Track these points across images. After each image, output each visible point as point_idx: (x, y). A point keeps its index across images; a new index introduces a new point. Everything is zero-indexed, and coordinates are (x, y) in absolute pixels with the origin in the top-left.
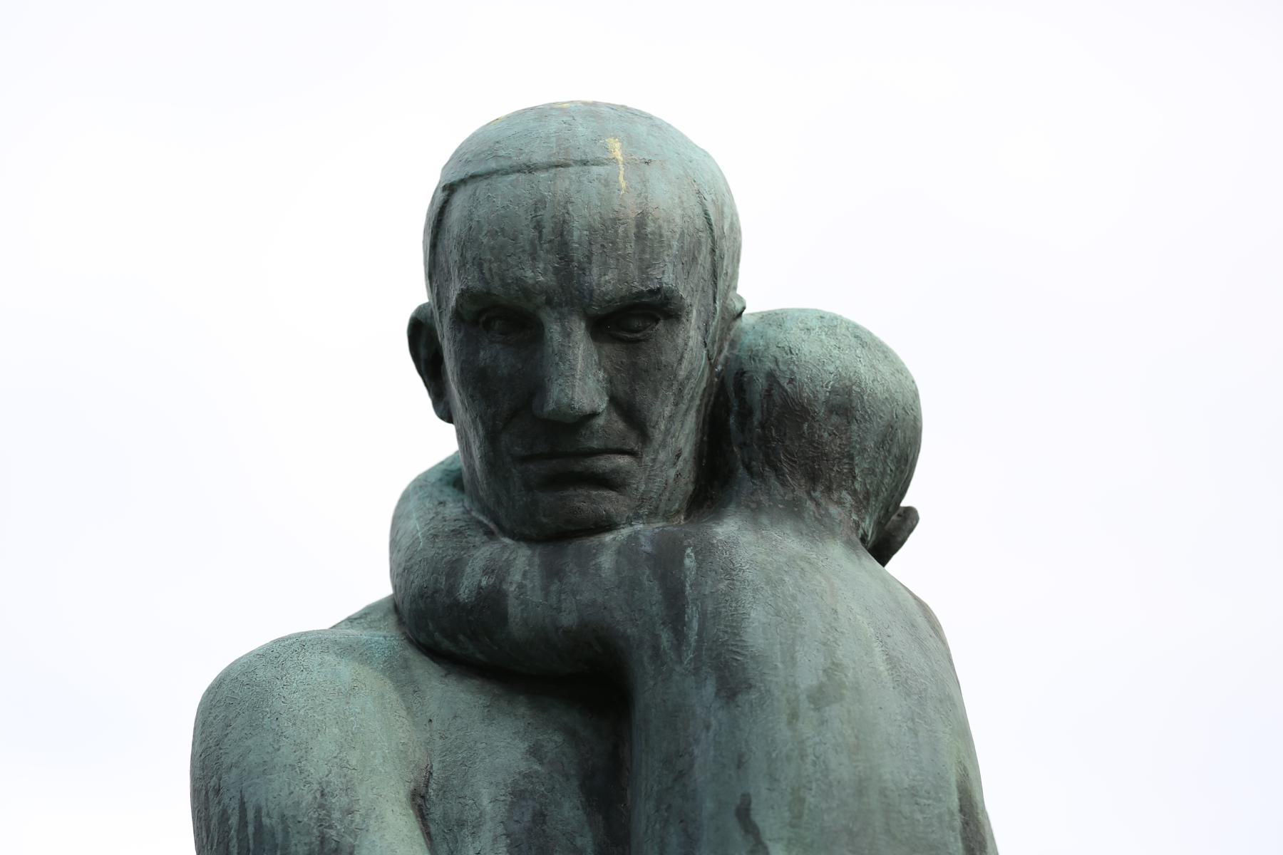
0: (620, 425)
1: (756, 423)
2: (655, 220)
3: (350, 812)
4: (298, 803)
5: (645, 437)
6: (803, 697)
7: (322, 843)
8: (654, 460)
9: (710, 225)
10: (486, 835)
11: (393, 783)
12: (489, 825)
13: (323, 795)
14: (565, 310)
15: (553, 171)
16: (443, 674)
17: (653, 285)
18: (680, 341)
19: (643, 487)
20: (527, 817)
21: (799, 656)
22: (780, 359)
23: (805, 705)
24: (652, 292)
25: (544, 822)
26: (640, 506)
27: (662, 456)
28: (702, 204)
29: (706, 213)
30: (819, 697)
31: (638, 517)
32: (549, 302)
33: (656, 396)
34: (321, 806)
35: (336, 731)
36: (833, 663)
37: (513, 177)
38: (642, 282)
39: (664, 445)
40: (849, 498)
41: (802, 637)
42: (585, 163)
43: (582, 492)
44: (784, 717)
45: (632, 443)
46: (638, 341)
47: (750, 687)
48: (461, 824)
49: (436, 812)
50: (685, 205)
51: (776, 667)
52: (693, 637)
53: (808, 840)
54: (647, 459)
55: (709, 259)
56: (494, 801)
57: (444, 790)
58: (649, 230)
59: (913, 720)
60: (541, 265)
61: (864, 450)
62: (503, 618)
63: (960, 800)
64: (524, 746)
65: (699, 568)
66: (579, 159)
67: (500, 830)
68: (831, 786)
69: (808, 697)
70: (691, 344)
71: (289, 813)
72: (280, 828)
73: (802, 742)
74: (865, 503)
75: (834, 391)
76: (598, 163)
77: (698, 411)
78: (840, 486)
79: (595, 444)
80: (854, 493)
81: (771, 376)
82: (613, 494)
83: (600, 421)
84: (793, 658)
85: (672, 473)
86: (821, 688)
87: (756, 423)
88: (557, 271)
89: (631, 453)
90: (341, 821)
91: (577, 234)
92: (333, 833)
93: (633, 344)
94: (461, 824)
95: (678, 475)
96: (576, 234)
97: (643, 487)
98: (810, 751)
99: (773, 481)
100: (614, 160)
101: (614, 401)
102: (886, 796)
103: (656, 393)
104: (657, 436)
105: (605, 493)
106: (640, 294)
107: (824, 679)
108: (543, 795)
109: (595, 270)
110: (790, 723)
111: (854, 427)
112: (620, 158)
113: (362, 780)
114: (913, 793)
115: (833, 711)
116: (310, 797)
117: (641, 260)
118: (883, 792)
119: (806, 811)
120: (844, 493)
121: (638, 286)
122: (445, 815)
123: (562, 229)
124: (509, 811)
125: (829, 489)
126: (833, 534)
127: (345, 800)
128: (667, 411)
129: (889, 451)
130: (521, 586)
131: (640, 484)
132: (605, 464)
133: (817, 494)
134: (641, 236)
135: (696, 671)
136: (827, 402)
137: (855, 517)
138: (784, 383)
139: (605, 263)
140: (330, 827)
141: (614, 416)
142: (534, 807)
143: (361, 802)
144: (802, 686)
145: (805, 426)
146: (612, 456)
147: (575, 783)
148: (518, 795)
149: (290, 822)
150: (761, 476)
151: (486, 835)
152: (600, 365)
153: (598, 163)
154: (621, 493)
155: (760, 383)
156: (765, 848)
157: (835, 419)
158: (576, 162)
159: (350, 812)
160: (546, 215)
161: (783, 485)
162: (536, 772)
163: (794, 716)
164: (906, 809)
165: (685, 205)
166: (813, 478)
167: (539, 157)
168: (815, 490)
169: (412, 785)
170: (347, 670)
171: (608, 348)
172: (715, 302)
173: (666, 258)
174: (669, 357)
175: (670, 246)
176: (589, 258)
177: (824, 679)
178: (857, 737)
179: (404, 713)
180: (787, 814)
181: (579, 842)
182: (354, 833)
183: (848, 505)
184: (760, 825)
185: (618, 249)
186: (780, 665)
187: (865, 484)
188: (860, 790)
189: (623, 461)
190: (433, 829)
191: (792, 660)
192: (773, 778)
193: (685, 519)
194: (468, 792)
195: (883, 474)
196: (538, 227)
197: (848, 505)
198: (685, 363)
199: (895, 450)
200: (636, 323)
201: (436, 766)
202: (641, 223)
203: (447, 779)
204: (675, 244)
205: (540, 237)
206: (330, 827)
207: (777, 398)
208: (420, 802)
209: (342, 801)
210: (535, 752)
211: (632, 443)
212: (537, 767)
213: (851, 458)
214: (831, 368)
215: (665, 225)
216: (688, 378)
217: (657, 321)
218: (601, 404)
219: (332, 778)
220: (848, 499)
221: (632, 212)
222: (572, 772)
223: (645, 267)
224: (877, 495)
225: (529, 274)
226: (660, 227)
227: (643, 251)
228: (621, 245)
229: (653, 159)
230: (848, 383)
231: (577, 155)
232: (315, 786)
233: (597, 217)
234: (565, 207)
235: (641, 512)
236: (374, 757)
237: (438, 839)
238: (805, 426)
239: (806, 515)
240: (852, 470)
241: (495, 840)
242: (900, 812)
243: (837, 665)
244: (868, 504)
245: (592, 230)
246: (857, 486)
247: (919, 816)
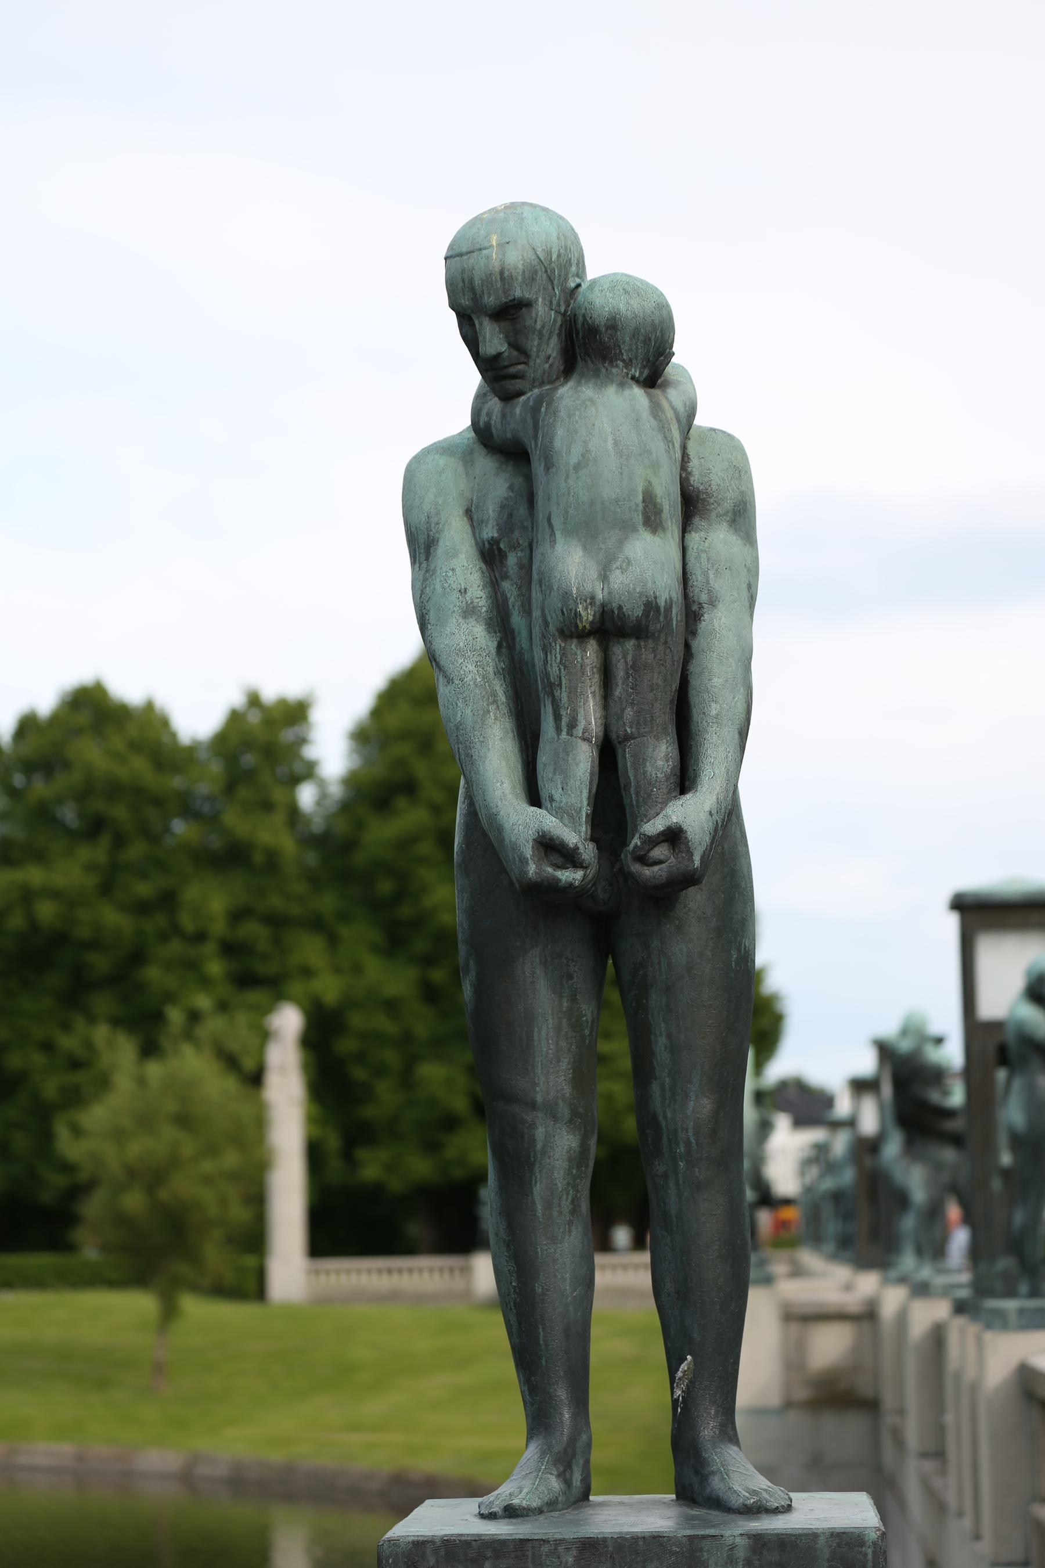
0: (515, 353)
1: (580, 337)
2: (508, 270)
3: (438, 524)
4: (420, 522)
5: (527, 356)
6: (571, 468)
7: (428, 537)
8: (535, 364)
9: (542, 262)
10: (490, 525)
11: (456, 508)
12: (491, 522)
13: (428, 518)
14: (479, 314)
15: (469, 255)
16: (486, 453)
17: (510, 298)
18: (534, 315)
19: (533, 375)
20: (505, 517)
21: (572, 450)
22: (587, 308)
23: (572, 471)
24: (511, 301)
25: (512, 518)
26: (534, 383)
27: (538, 361)
28: (536, 253)
29: (538, 257)
30: (577, 467)
31: (534, 387)
32: (472, 311)
33: (528, 339)
34: (428, 523)
35: (434, 489)
36: (586, 450)
37: (456, 259)
38: (506, 297)
39: (538, 356)
40: (621, 363)
41: (575, 441)
42: (480, 250)
43: (508, 382)
44: (564, 478)
45: (523, 359)
46: (515, 319)
47: (554, 465)
48: (482, 522)
49: (475, 518)
50: (525, 258)
51: (563, 456)
52: (539, 444)
53: (569, 529)
54: (531, 364)
55: (545, 275)
56: (494, 511)
57: (477, 508)
58: (506, 275)
59: (621, 468)
60: (467, 297)
61: (625, 342)
62: (491, 434)
63: (643, 497)
64: (507, 485)
65: (546, 412)
66: (478, 248)
67: (495, 523)
68: (579, 504)
69: (574, 468)
70: (540, 313)
71: (418, 526)
72: (416, 532)
73: (569, 488)
74: (630, 363)
75: (608, 320)
76: (485, 248)
77: (559, 335)
78: (616, 360)
79: (506, 363)
80: (624, 361)
81: (584, 316)
82: (520, 381)
83: (506, 354)
84: (570, 451)
85: (547, 366)
86: (579, 463)
87: (580, 337)
88: (472, 299)
89: (523, 363)
90: (434, 528)
91: (477, 282)
92: (432, 533)
93: (513, 320)
94: (482, 522)
95: (551, 366)
96: (476, 283)
97: (533, 375)
98: (572, 491)
99: (589, 362)
100: (491, 246)
101: (510, 344)
102: (604, 504)
103: (527, 338)
104: (533, 354)
105: (517, 381)
106: (506, 303)
107: (581, 459)
108: (512, 506)
109: (486, 297)
110: (565, 480)
111: (619, 333)
112: (495, 244)
113: (443, 510)
114: (617, 501)
115: (583, 472)
116: (424, 519)
117: (504, 289)
118: (602, 503)
119: (569, 517)
120: (619, 362)
121: (504, 300)
122: (478, 519)
123: (471, 280)
124: (499, 514)
125: (611, 362)
126: (612, 381)
127: (436, 519)
128: (536, 343)
129: (638, 339)
130: (495, 421)
131: (530, 374)
132: (512, 370)
133: (606, 365)
134: (502, 278)
135: (539, 460)
136: (605, 325)
137: (625, 371)
138: (588, 319)
139: (489, 293)
140: (431, 531)
141: (512, 350)
142: (508, 512)
143: (442, 519)
144: (572, 464)
145: (598, 337)
146: (515, 366)
147: (525, 499)
148: (503, 507)
149: (418, 529)
150: (586, 362)
151: (490, 525)
152: (500, 332)
153: (485, 248)
154: (524, 379)
155: (580, 319)
156: (555, 533)
157: (609, 332)
158: (477, 250)
159: (438, 524)
160: (465, 276)
161: (592, 363)
162: (511, 496)
163: (567, 477)
164: (612, 508)
165: (525, 258)
166: (604, 358)
167: (464, 250)
168: (605, 363)
169: (466, 508)
170: (442, 461)
171: (503, 324)
172: (554, 290)
173: (516, 285)
174: (529, 323)
175: (517, 279)
176: (483, 291)
177: (581, 459)
178: (592, 482)
179: (464, 476)
180: (562, 519)
181: (525, 524)
182: (438, 532)
183: (621, 367)
184: (554, 524)
185: (493, 286)
186: (564, 455)
187: (628, 356)
188: (592, 504)
189: (521, 367)
190: (475, 525)
191: (569, 452)
192: (558, 504)
193: (564, 379)
194: (485, 508)
195: (637, 349)
196: (463, 281)
197: (621, 367)
198: (539, 323)
199: (641, 338)
200: (513, 312)
201: (475, 497)
202: (502, 273)
203: (478, 503)
204: (520, 278)
205: (464, 286)
206: (431, 531)
207: (586, 326)
208: (468, 513)
209: (434, 520)
210: (511, 488)
211: (523, 359)
212: (511, 494)
213: (619, 346)
214: (607, 309)
215: (513, 271)
216: (543, 327)
217: (522, 309)
218: (504, 348)
219: (432, 510)
220: (621, 364)
221: (497, 269)
222: (525, 494)
223: (505, 292)
224: (636, 359)
225: (463, 301)
226: (511, 272)
227: (505, 285)
228: (495, 284)
229: (510, 240)
230: (614, 315)
231: (477, 246)
232: (426, 515)
233: (483, 274)
234: (472, 272)
235: (535, 385)
236: (449, 498)
237: (476, 528)
238: (598, 337)
239: (601, 375)
240: (621, 351)
241: (493, 528)
242: (610, 510)
243: (588, 451)
244: (632, 363)
245: (482, 280)
246: (625, 357)
247: (619, 510)
